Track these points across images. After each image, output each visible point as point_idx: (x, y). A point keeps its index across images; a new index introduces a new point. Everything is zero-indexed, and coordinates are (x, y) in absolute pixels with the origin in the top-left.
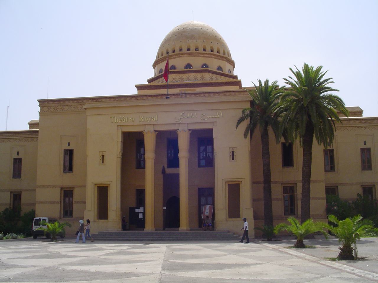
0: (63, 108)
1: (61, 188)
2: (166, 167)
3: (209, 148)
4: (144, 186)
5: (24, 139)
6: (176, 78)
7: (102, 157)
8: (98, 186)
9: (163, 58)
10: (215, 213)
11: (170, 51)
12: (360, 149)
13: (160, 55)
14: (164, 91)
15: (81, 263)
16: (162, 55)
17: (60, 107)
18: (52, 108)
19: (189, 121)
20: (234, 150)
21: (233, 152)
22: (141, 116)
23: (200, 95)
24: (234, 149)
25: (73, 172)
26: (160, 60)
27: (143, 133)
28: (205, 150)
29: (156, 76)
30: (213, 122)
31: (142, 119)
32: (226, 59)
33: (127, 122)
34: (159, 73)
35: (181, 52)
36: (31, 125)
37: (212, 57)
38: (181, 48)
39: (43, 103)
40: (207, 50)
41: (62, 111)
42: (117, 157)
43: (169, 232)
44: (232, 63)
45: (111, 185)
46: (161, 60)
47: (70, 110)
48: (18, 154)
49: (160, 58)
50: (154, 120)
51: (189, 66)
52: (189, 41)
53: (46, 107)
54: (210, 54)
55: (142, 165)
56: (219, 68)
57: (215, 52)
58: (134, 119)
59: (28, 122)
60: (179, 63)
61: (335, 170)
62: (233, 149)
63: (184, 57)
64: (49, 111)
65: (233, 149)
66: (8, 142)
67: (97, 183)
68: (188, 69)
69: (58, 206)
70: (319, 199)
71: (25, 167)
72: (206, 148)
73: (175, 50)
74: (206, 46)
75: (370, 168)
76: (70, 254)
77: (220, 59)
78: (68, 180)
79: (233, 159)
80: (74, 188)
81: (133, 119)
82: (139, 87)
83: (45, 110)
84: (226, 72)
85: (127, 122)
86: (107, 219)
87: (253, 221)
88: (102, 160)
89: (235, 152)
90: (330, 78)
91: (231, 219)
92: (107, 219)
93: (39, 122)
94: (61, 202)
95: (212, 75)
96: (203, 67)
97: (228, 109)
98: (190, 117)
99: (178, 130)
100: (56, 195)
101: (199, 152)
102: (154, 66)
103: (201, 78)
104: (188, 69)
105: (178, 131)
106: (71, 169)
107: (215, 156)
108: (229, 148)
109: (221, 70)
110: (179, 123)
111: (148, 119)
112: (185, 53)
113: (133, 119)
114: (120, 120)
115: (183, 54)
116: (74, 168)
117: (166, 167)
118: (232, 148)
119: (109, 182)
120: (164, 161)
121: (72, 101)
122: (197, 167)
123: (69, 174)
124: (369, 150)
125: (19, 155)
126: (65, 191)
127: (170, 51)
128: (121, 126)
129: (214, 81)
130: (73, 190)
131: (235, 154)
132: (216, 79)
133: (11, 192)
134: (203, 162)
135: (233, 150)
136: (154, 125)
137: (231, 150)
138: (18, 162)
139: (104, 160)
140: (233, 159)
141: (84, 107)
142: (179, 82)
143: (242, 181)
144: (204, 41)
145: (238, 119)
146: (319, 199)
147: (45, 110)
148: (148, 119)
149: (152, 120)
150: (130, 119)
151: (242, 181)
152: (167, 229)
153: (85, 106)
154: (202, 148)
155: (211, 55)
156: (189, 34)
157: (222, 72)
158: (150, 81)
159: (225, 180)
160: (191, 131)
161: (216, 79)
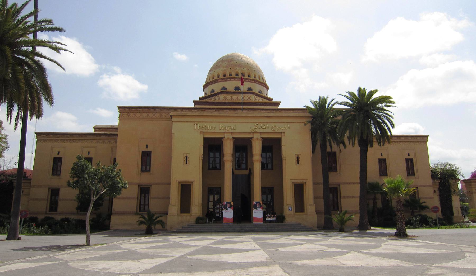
0: (160, 115)
1: (49, 188)
5: (95, 140)
6: (227, 97)
7: (185, 158)
8: (182, 183)
9: (215, 81)
10: (284, 208)
11: (228, 74)
12: (378, 159)
14: (240, 107)
17: (139, 114)
18: (131, 114)
19: (261, 131)
20: (300, 156)
21: (187, 157)
22: (221, 125)
24: (299, 155)
27: (222, 139)
29: (207, 95)
30: (281, 133)
31: (222, 127)
32: (264, 85)
33: (201, 129)
34: (211, 93)
37: (255, 83)
39: (122, 109)
40: (251, 76)
41: (148, 117)
42: (200, 159)
43: (243, 225)
44: (267, 88)
45: (194, 183)
47: (161, 117)
49: (208, 82)
50: (207, 128)
51: (224, 88)
52: (237, 68)
53: (145, 113)
56: (260, 91)
58: (215, 127)
59: (94, 126)
60: (217, 87)
61: (415, 174)
62: (186, 155)
63: (233, 80)
64: (135, 117)
66: (97, 143)
68: (237, 91)
73: (225, 75)
74: (250, 73)
75: (413, 174)
77: (260, 85)
78: (145, 179)
79: (298, 163)
81: (214, 127)
82: (195, 103)
83: (144, 116)
84: (264, 95)
85: (209, 129)
86: (190, 213)
87: (316, 215)
88: (185, 161)
89: (300, 158)
92: (190, 213)
93: (118, 126)
94: (341, 198)
95: (256, 96)
96: (248, 90)
97: (293, 123)
98: (263, 128)
99: (224, 137)
102: (204, 87)
103: (247, 99)
104: (237, 91)
105: (224, 138)
108: (184, 154)
109: (261, 92)
110: (254, 133)
111: (227, 127)
112: (234, 78)
113: (214, 127)
114: (203, 127)
115: (232, 78)
121: (152, 110)
124: (411, 160)
125: (89, 155)
127: (228, 74)
128: (203, 132)
129: (257, 101)
131: (299, 159)
132: (255, 99)
133: (139, 186)
136: (232, 132)
137: (185, 156)
140: (298, 163)
141: (171, 114)
143: (193, 182)
146: (353, 197)
147: (144, 116)
148: (227, 127)
149: (231, 128)
150: (211, 127)
153: (172, 114)
154: (212, 154)
157: (261, 94)
158: (201, 99)
159: (292, 180)
161: (255, 99)
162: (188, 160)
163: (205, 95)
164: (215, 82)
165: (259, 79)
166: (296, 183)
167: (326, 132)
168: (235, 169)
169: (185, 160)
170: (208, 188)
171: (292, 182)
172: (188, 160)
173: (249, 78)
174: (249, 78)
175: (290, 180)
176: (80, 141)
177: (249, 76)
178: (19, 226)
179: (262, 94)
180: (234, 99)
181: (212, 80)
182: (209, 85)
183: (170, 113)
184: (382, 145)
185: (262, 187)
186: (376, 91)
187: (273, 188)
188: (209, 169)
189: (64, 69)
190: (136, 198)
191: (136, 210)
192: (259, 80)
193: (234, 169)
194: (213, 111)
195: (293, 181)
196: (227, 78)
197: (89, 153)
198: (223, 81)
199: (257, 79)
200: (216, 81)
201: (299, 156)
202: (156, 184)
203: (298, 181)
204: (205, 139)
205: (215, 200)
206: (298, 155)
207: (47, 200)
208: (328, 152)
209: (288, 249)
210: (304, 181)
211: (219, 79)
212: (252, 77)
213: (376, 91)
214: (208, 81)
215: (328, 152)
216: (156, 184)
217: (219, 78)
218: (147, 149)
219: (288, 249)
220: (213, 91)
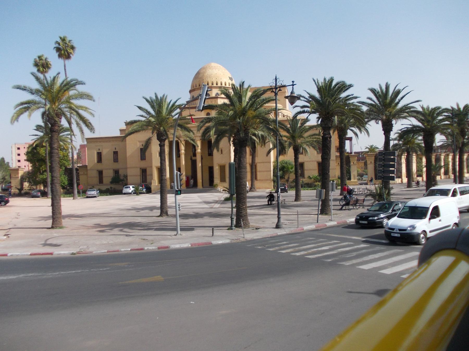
1: (140, 168)
2: (192, 156)
4: (180, 166)
15: (146, 203)
20: (222, 149)
36: (121, 131)
40: (214, 84)
48: (115, 149)
55: (117, 161)
67: (220, 164)
69: (139, 177)
71: (120, 156)
76: (197, 204)
78: (143, 164)
79: (222, 153)
90: (397, 85)
100: (138, 172)
117: (192, 156)
120: (192, 154)
126: (142, 169)
131: (223, 151)
133: (113, 170)
134: (115, 161)
138: (116, 153)
140: (222, 153)
142: (56, 138)
145: (152, 141)
158: (188, 102)
167: (254, 109)
173: (217, 86)
176: (110, 141)
177: (217, 84)
185: (212, 155)
186: (82, 83)
189: (179, 99)
191: (140, 182)
196: (198, 88)
197: (115, 149)
202: (259, 163)
205: (412, 134)
207: (140, 176)
208: (120, 135)
209: (108, 228)
213: (82, 83)
215: (120, 135)
216: (259, 163)
219: (108, 228)
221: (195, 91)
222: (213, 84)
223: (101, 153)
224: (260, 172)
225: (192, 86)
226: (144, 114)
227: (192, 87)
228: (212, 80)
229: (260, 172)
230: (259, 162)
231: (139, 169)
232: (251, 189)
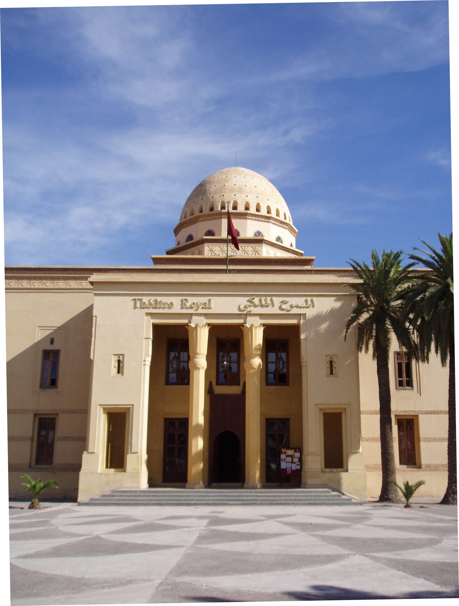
3: (183, 355)
7: (329, 363)
9: (194, 219)
13: (183, 217)
16: (185, 217)
20: (334, 359)
21: (331, 362)
23: (352, 274)
24: (333, 357)
25: (57, 388)
26: (190, 221)
28: (178, 358)
35: (212, 212)
38: (212, 206)
46: (190, 222)
50: (207, 306)
54: (266, 216)
57: (273, 214)
65: (331, 357)
69: (28, 444)
70: (435, 440)
72: (179, 355)
74: (203, 205)
79: (332, 373)
80: (58, 414)
89: (335, 363)
91: (328, 470)
94: (32, 438)
101: (168, 362)
106: (54, 383)
107: (303, 367)
108: (326, 355)
116: (61, 382)
118: (330, 356)
119: (343, 406)
122: (265, 384)
123: (51, 392)
126: (40, 419)
130: (55, 418)
131: (334, 365)
132: (268, 252)
134: (173, 376)
135: (331, 360)
137: (328, 359)
139: (334, 369)
140: (332, 373)
141: (90, 280)
143: (345, 409)
144: (257, 197)
146: (435, 440)
151: (345, 409)
152: (214, 484)
154: (172, 355)
155: (268, 218)
156: (235, 185)
159: (319, 406)
160: (211, 326)
161: (268, 252)
162: (335, 367)
163: (178, 245)
164: (194, 221)
165: (278, 214)
166: (327, 411)
168: (218, 384)
169: (328, 367)
170: (166, 420)
171: (320, 409)
172: (335, 367)
173: (258, 213)
174: (258, 213)
175: (316, 405)
177: (258, 210)
178: (434, 498)
179: (282, 242)
180: (217, 253)
181: (189, 217)
182: (183, 228)
183: (90, 277)
184: (391, 336)
187: (288, 419)
188: (168, 383)
190: (30, 438)
191: (28, 461)
192: (277, 218)
193: (214, 383)
194: (342, 274)
195: (322, 407)
198: (208, 220)
199: (273, 214)
200: (196, 219)
201: (333, 359)
202: (427, 413)
203: (332, 406)
204: (156, 328)
206: (331, 357)
210: (343, 406)
211: (246, 214)
212: (264, 212)
214: (184, 220)
216: (427, 413)
217: (201, 214)
218: (52, 346)
220: (190, 238)
221: (197, 222)
222: (247, 208)
223: (56, 353)
224: (428, 440)
225: (184, 215)
226: (434, 255)
227: (188, 215)
228: (269, 203)
229: (428, 440)
230: (426, 409)
231: (30, 417)
232: (202, 530)
